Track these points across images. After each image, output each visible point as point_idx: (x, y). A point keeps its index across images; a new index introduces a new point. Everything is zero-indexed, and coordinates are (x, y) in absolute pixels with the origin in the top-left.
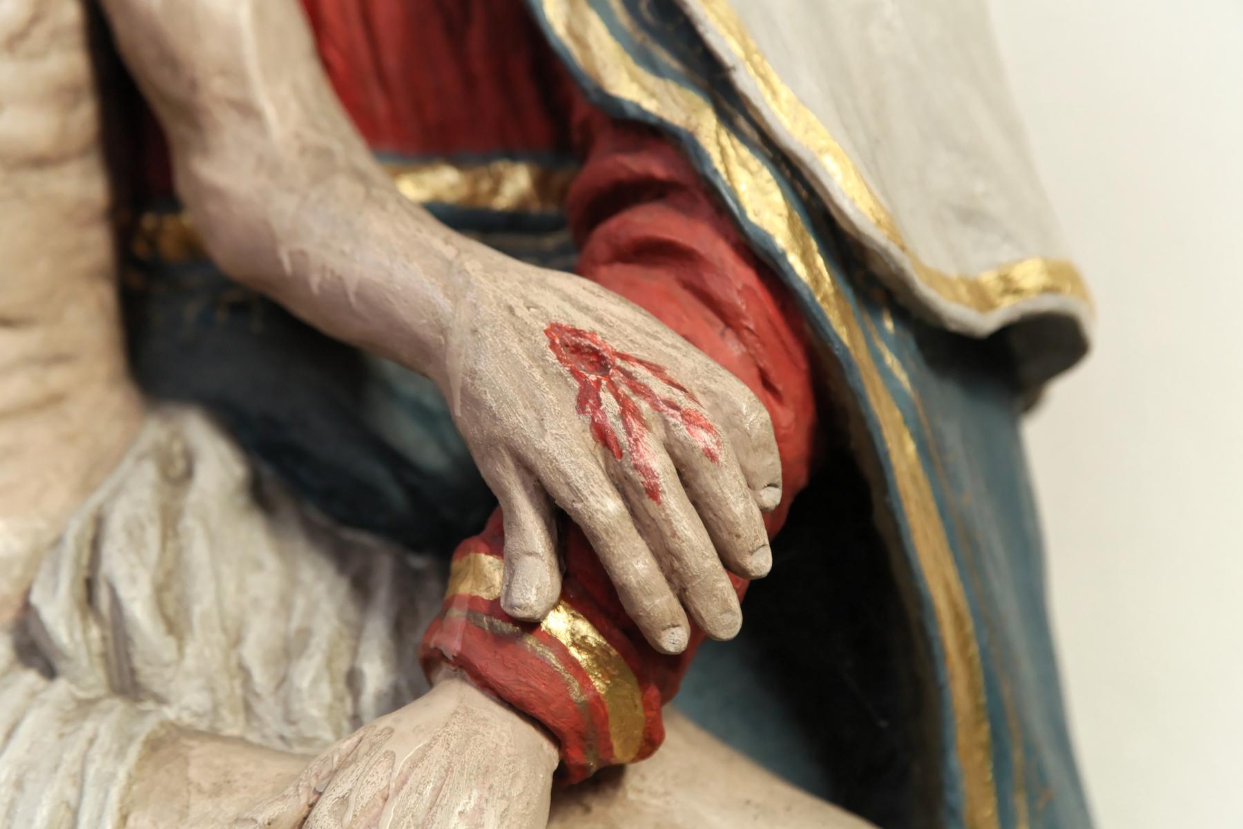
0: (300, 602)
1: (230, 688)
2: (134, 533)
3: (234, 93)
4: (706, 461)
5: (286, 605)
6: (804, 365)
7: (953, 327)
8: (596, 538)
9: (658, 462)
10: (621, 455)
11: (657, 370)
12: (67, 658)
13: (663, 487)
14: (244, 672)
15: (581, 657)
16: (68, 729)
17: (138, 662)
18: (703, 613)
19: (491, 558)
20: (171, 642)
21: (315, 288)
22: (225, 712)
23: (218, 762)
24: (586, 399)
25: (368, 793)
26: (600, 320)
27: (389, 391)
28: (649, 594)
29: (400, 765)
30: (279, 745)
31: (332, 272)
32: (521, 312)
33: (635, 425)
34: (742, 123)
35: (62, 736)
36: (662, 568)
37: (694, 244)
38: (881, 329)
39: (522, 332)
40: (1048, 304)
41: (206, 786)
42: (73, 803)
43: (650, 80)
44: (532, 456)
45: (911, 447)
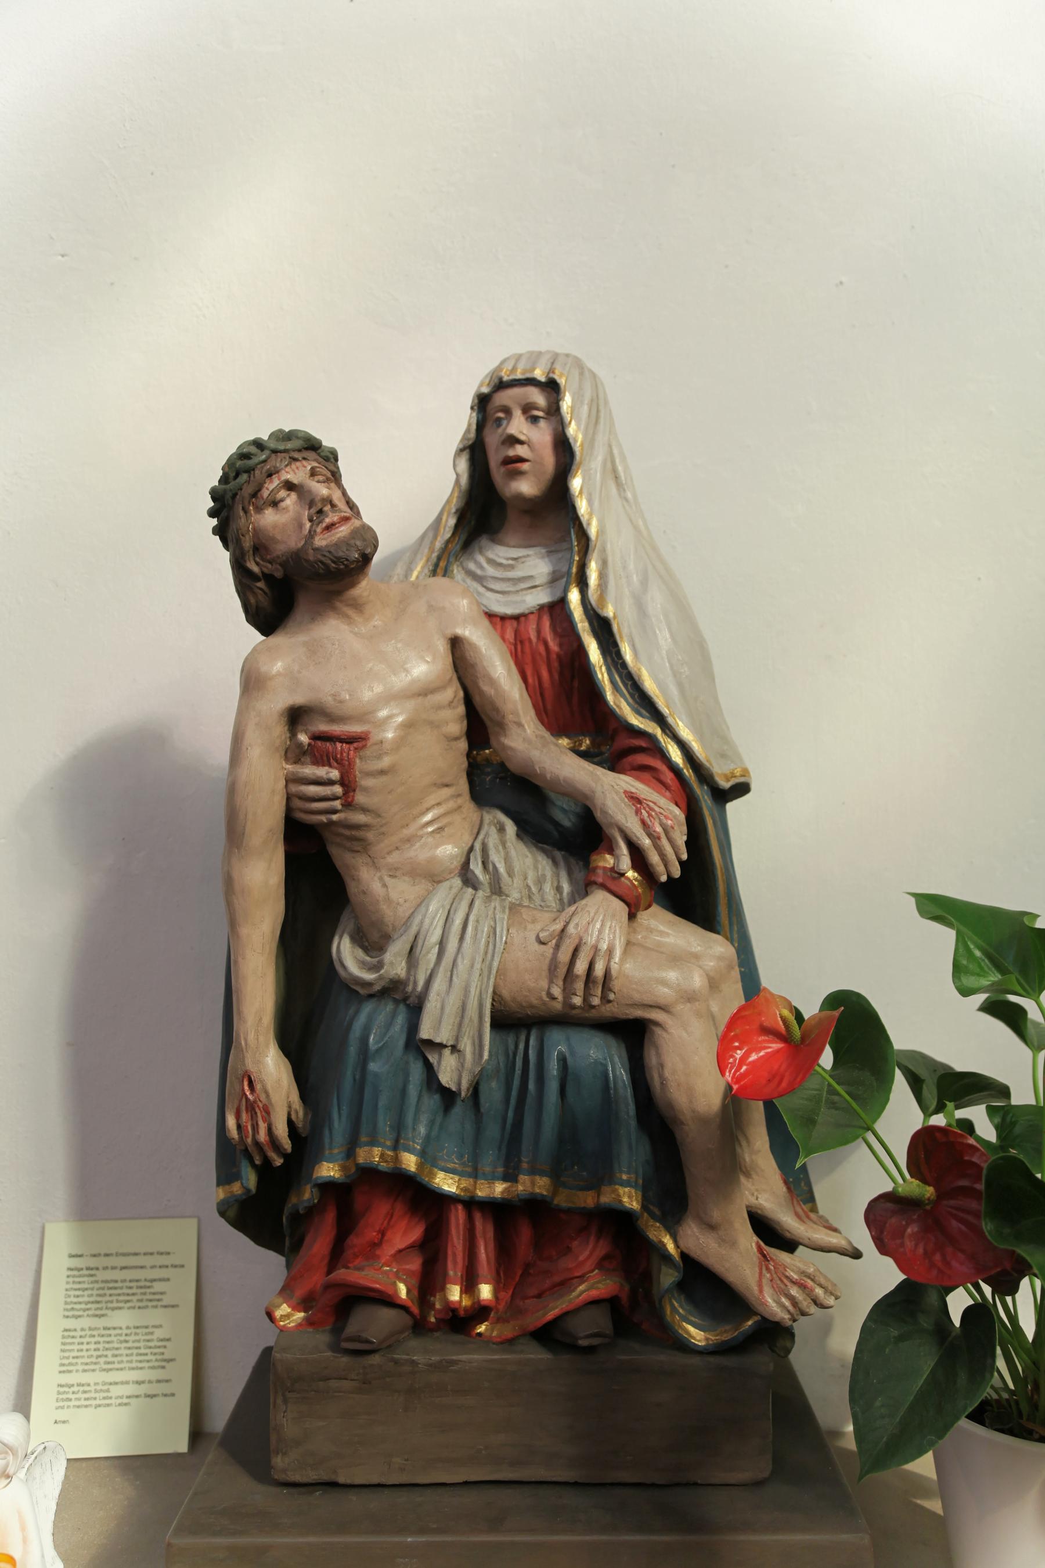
0: (540, 867)
1: (525, 892)
2: (496, 848)
3: (516, 720)
4: (671, 829)
5: (536, 868)
6: (686, 800)
7: (721, 787)
8: (644, 851)
9: (659, 829)
10: (649, 827)
11: (655, 803)
12: (482, 884)
13: (662, 836)
14: (528, 886)
15: (636, 883)
16: (487, 905)
17: (502, 885)
18: (671, 871)
19: (609, 856)
20: (510, 879)
21: (549, 778)
22: (524, 899)
23: (530, 913)
24: (638, 812)
25: (585, 922)
26: (637, 789)
27: (553, 803)
28: (658, 866)
29: (592, 914)
30: (540, 908)
31: (555, 774)
32: (616, 787)
33: (652, 819)
34: (667, 731)
35: (486, 907)
36: (661, 859)
37: (657, 766)
38: (704, 788)
39: (617, 793)
40: (742, 780)
41: (530, 920)
42: (493, 926)
43: (641, 719)
44: (624, 828)
45: (711, 821)
